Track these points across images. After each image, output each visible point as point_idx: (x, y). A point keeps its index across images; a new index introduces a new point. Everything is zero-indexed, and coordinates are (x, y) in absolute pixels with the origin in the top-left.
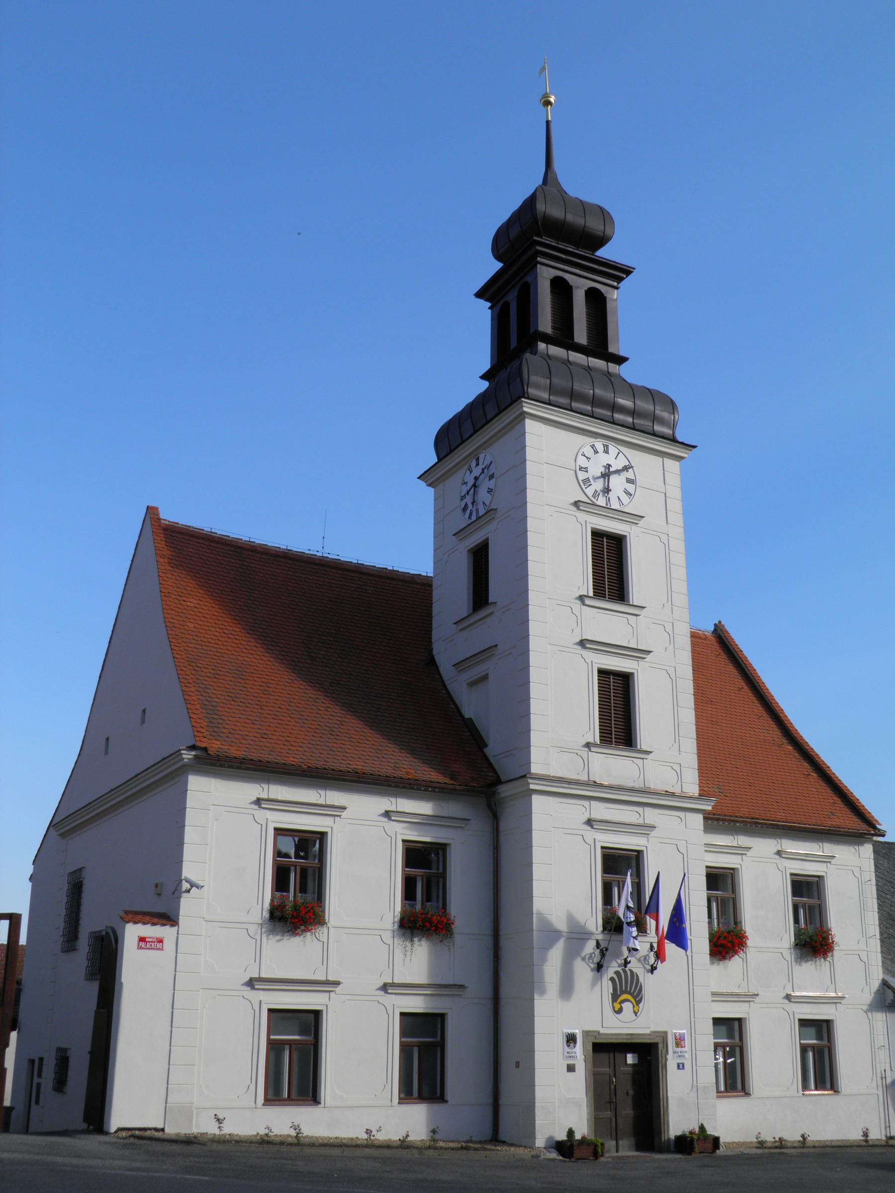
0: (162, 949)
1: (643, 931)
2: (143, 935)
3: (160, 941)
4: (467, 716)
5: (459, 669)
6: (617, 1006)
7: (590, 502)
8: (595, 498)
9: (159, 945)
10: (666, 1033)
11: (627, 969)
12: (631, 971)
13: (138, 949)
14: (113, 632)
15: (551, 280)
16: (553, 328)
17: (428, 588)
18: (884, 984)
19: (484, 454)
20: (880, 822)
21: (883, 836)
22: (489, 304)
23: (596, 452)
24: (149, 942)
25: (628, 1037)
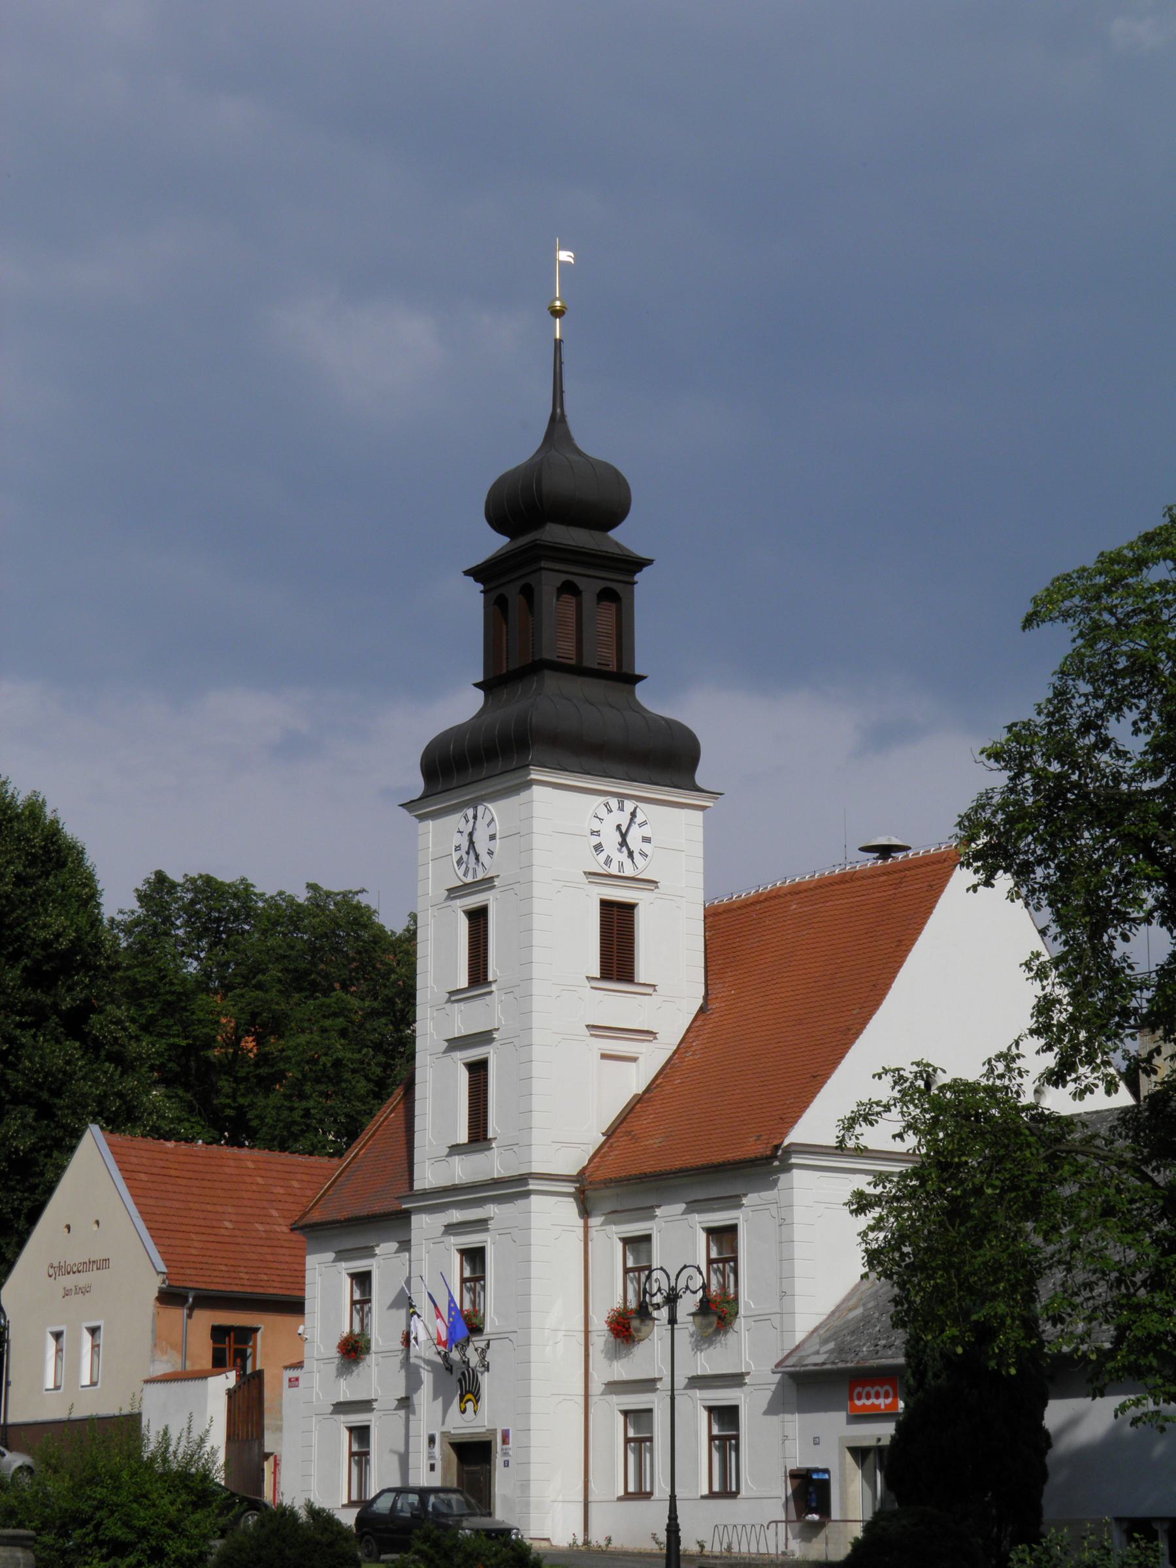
6: (463, 1406)
23: (610, 811)
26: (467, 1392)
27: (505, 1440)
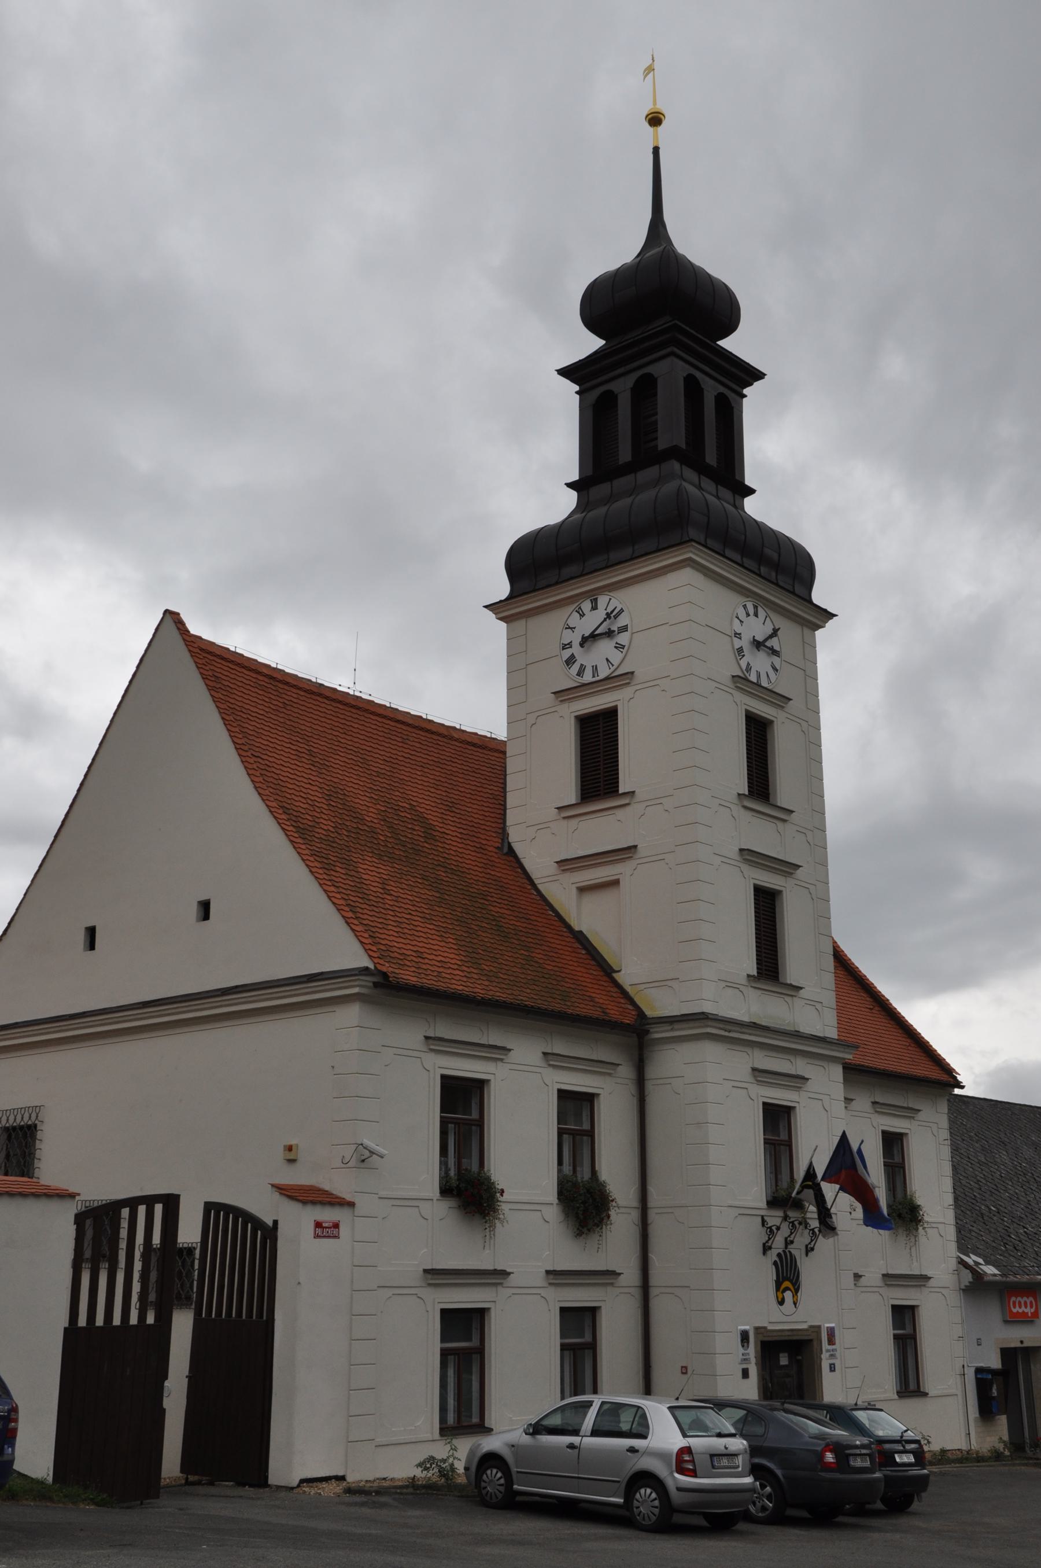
0: (337, 1237)
1: (31, 1176)
2: (320, 1219)
3: (336, 1226)
4: (577, 929)
5: (563, 868)
6: (780, 1296)
7: (743, 676)
8: (747, 672)
9: (335, 1231)
10: (819, 1327)
11: (787, 1251)
12: (790, 1252)
13: (314, 1237)
14: (86, 776)
15: (715, 396)
16: (687, 443)
17: (501, 755)
18: (959, 1263)
19: (609, 597)
20: (957, 1070)
21: (963, 1087)
22: (577, 388)
23: (748, 615)
24: (326, 1228)
25: (789, 1333)
26: (785, 1279)
27: (831, 1341)
